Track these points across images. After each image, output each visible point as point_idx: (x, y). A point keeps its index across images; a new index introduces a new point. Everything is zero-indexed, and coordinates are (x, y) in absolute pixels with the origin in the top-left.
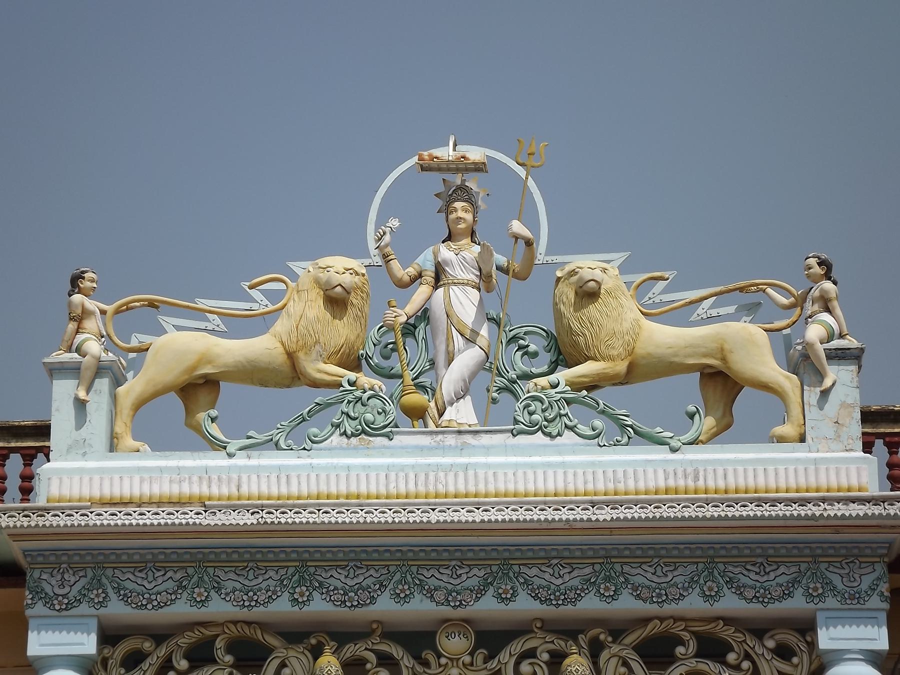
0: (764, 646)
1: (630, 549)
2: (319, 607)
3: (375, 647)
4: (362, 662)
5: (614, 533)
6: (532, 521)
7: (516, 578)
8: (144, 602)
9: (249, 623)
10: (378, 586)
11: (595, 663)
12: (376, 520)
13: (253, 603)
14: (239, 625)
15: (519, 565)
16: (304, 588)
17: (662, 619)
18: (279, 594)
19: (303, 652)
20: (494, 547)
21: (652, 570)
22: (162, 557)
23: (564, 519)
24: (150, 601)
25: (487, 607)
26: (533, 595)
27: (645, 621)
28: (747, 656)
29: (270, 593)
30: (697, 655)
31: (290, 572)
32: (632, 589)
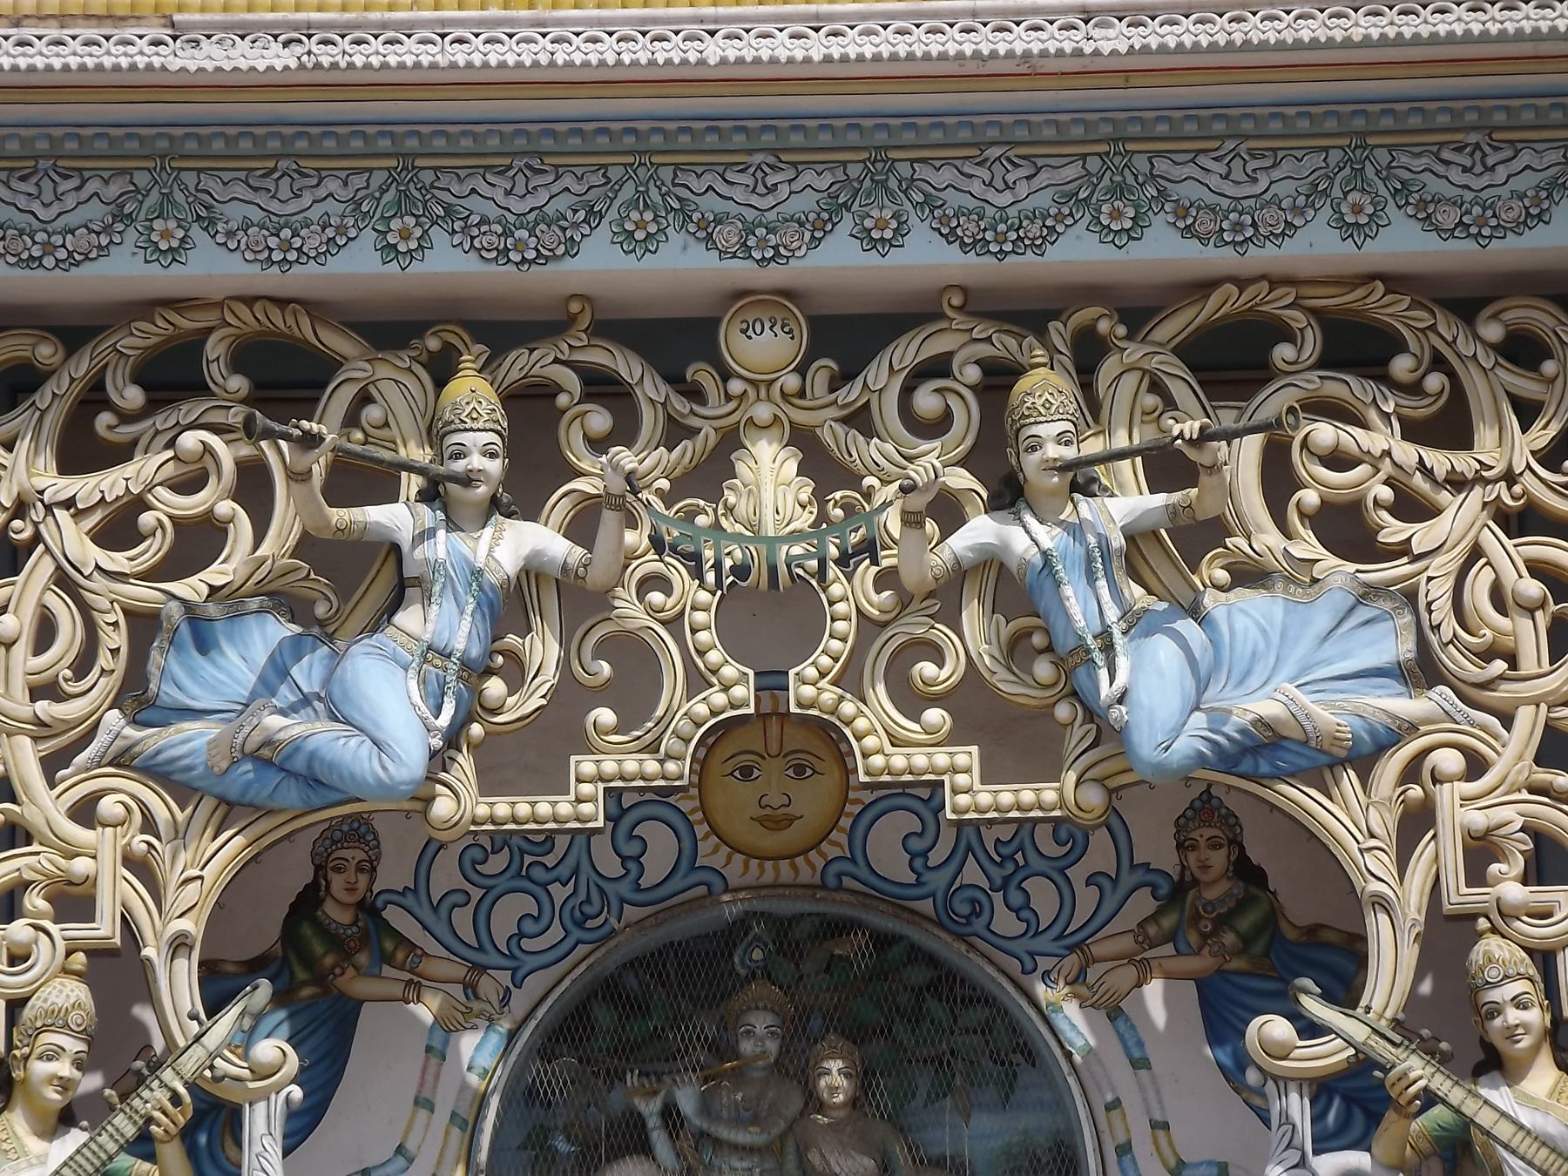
0: (1476, 337)
1: (1169, 119)
2: (447, 263)
3: (578, 356)
4: (548, 391)
5: (1133, 82)
6: (943, 57)
7: (905, 192)
9: (282, 302)
10: (582, 215)
11: (1087, 386)
12: (578, 58)
13: (292, 256)
14: (258, 307)
15: (912, 161)
16: (411, 221)
17: (1242, 283)
20: (853, 120)
21: (1220, 168)
22: (72, 146)
23: (1019, 51)
24: (49, 249)
25: (839, 261)
27: (1204, 287)
28: (1438, 362)
29: (330, 232)
31: (375, 184)
32: (1175, 212)
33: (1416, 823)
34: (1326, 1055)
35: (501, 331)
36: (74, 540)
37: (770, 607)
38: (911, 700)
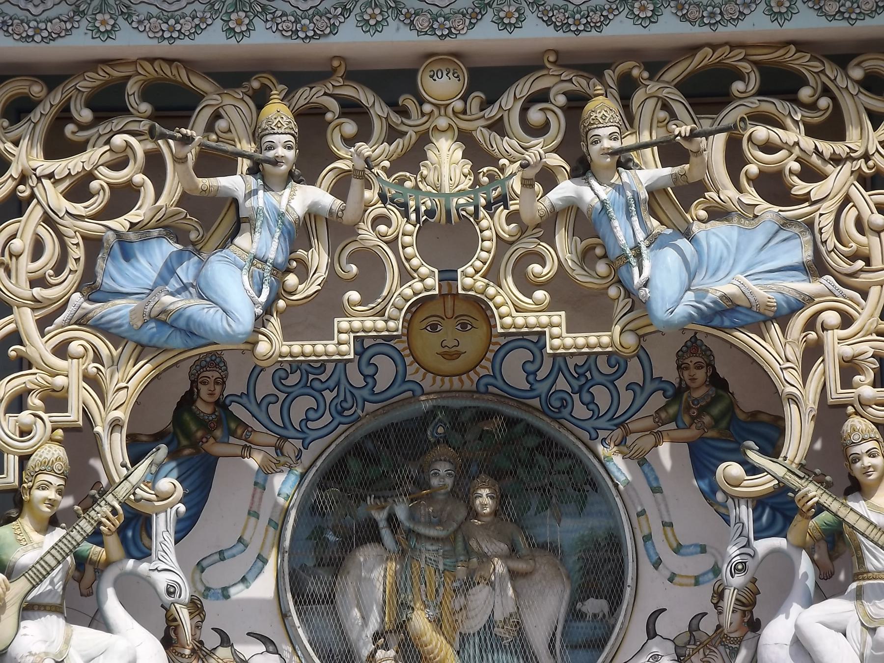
0: (848, 77)
2: (263, 39)
4: (321, 111)
8: (31, 33)
9: (170, 61)
10: (339, 10)
13: (175, 35)
14: (156, 64)
17: (714, 47)
18: (209, 21)
19: (242, 99)
24: (38, 31)
25: (485, 36)
26: (545, 18)
27: (692, 49)
28: (826, 91)
29: (197, 21)
30: (760, 92)
32: (676, 7)
33: (813, 353)
34: (762, 484)
35: (294, 77)
36: (54, 197)
37: (446, 234)
38: (527, 286)
